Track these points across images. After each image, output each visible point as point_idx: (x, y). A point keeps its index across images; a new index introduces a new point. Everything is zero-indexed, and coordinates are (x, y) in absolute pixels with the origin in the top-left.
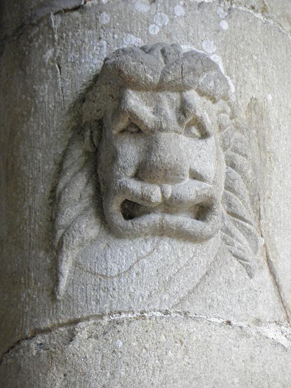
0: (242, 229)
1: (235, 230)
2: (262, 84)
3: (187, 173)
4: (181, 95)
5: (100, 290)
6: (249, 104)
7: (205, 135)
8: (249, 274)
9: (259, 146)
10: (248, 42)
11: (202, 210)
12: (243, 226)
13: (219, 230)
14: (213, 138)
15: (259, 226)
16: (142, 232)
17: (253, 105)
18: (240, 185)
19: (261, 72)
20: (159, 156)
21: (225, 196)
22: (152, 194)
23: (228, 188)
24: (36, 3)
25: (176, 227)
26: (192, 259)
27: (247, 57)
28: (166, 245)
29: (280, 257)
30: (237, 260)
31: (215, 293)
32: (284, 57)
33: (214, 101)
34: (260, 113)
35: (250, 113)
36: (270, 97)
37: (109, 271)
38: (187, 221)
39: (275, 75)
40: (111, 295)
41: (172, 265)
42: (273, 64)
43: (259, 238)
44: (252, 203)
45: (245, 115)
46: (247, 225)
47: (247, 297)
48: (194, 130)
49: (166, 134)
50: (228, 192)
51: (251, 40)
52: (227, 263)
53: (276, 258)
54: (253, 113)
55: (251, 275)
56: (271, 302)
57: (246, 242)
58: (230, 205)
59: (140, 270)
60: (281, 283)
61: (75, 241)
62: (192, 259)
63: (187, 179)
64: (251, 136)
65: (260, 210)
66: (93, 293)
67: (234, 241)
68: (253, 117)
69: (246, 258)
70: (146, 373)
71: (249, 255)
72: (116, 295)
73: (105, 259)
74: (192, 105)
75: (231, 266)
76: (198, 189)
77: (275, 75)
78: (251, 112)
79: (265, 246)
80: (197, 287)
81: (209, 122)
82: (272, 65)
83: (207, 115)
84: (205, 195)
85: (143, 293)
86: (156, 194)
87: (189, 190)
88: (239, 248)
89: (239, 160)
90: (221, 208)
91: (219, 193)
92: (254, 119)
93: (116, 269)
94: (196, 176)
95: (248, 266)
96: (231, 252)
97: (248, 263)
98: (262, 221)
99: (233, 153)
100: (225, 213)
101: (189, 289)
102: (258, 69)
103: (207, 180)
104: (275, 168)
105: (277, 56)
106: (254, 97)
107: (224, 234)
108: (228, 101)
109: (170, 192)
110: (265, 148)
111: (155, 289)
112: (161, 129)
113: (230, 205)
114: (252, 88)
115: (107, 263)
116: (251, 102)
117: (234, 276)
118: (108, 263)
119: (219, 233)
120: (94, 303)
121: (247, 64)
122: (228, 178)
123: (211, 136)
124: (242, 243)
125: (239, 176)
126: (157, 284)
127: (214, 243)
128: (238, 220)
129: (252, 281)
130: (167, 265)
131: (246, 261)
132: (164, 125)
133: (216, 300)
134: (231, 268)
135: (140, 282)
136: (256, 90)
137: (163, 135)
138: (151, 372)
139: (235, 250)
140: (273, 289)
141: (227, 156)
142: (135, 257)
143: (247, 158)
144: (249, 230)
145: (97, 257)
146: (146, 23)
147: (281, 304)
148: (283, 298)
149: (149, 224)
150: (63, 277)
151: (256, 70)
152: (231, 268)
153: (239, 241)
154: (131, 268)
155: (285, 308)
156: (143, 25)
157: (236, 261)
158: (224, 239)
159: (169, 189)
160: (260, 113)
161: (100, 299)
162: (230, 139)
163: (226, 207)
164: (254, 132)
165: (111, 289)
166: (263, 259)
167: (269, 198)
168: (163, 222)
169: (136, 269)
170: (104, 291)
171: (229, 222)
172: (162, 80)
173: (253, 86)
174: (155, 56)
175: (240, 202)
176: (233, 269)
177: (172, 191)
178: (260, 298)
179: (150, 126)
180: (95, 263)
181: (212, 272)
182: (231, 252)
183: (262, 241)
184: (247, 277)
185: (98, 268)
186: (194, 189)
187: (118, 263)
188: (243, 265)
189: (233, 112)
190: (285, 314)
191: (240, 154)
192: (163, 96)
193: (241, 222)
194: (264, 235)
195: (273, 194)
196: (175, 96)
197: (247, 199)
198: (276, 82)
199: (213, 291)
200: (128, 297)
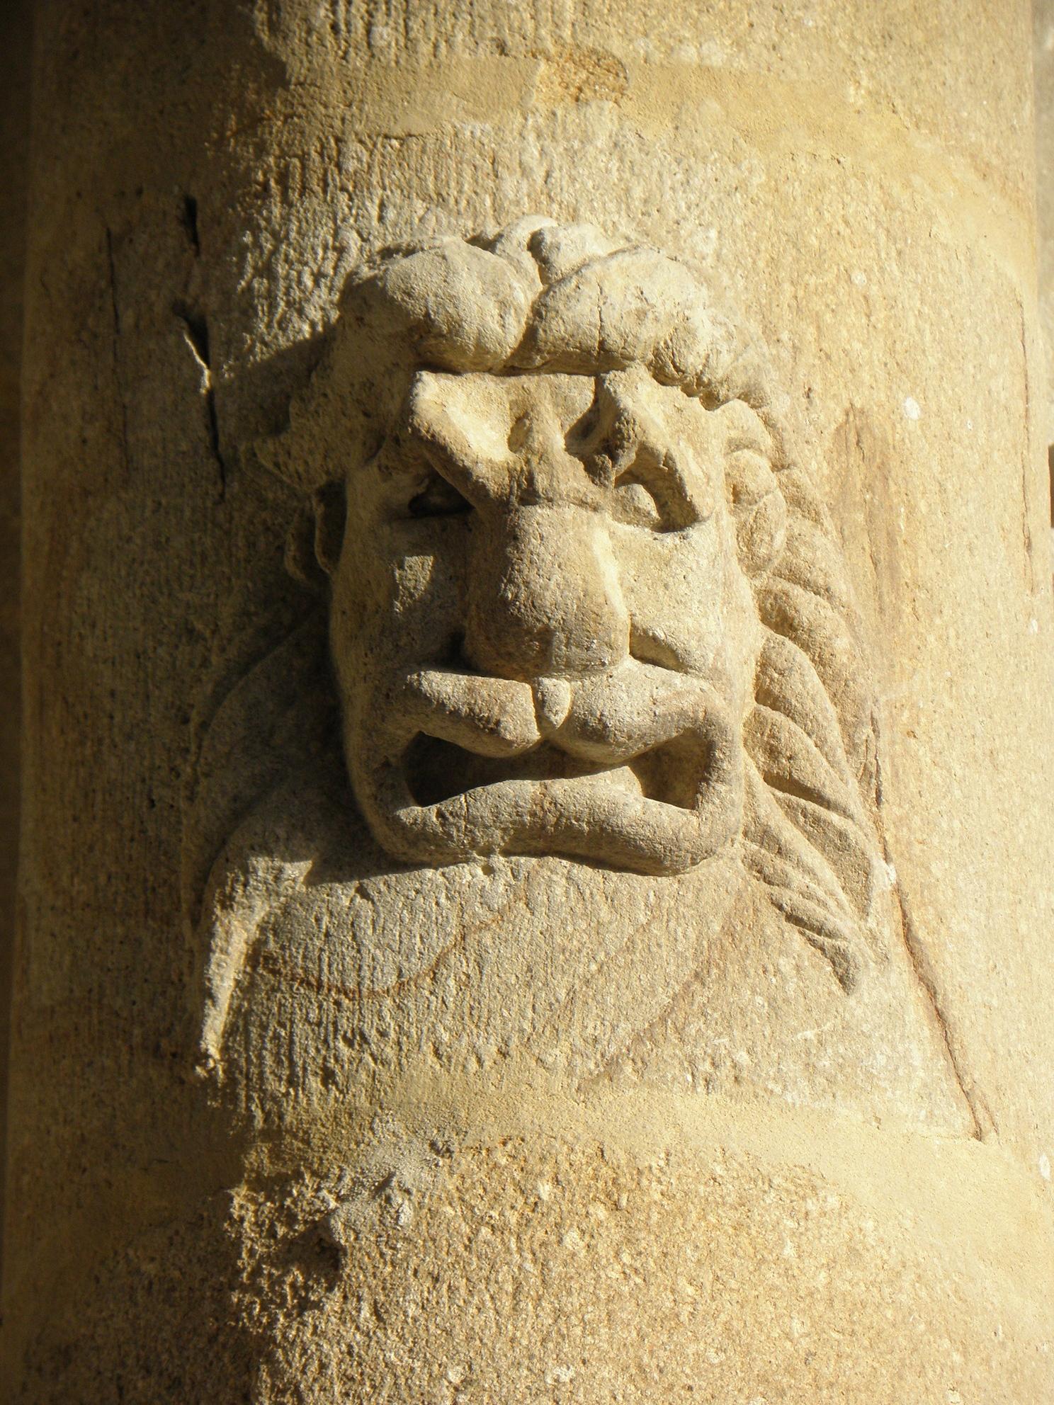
0: (816, 830)
1: (790, 834)
2: (886, 365)
3: (623, 641)
4: (599, 383)
5: (335, 1038)
6: (838, 430)
7: (676, 514)
8: (841, 980)
9: (875, 564)
10: (835, 226)
11: (678, 765)
12: (817, 821)
13: (735, 833)
14: (709, 526)
15: (877, 822)
16: (474, 844)
17: (856, 434)
18: (805, 682)
19: (879, 326)
20: (527, 584)
21: (757, 723)
22: (503, 709)
23: (765, 696)
24: (325, 477)
25: (588, 823)
26: (645, 928)
27: (830, 278)
28: (557, 874)
29: (949, 928)
30: (803, 934)
31: (725, 1040)
32: (959, 282)
33: (712, 401)
34: (878, 460)
35: (843, 458)
36: (912, 408)
37: (368, 974)
38: (617, 793)
39: (928, 337)
40: (372, 1055)
41: (580, 951)
42: (922, 301)
43: (875, 862)
44: (852, 749)
45: (825, 464)
46: (834, 817)
47: (837, 1053)
48: (645, 500)
49: (548, 511)
50: (767, 711)
51: (847, 223)
52: (764, 943)
53: (935, 932)
54: (855, 457)
55: (845, 981)
56: (921, 1074)
57: (827, 873)
58: (773, 753)
59: (472, 970)
60: (953, 1013)
61: (252, 882)
62: (645, 928)
63: (629, 664)
64: (846, 533)
65: (878, 771)
66: (312, 1052)
67: (789, 869)
68: (855, 470)
69: (829, 926)
70: (489, 1304)
71: (842, 919)
72: (390, 1052)
73: (354, 937)
74: (534, 303)
75: (781, 953)
76: (662, 693)
77: (928, 337)
78: (848, 453)
79: (898, 890)
80: (663, 1020)
81: (702, 478)
82: (918, 304)
83: (691, 452)
84: (682, 713)
85: (481, 1042)
86: (515, 708)
87: (634, 698)
88: (807, 895)
89: (805, 605)
90: (741, 766)
91: (734, 710)
92: (858, 480)
93: (390, 968)
94: (651, 650)
95: (838, 951)
96: (780, 908)
97: (838, 943)
98: (890, 811)
99: (787, 586)
100: (758, 779)
101: (638, 1025)
102: (868, 316)
103: (692, 663)
104: (931, 638)
105: (935, 278)
106: (858, 405)
107: (755, 847)
108: (764, 409)
109: (567, 704)
110: (893, 569)
111: (522, 1031)
112: (530, 496)
113: (773, 753)
114: (850, 375)
115: (359, 951)
116: (847, 421)
117: (791, 987)
118: (363, 950)
119: (737, 845)
120: (315, 1083)
121: (831, 298)
122: (765, 664)
123: (704, 520)
124: (815, 876)
125: (803, 658)
126: (530, 1014)
127: (724, 874)
128: (802, 802)
129: (852, 1002)
130: (563, 951)
131: (830, 935)
132: (541, 482)
133: (729, 1063)
134: (782, 961)
135: (472, 1008)
136: (862, 383)
137: (539, 514)
138: (507, 1303)
139: (789, 898)
140: (927, 1032)
141: (763, 594)
142: (453, 929)
143: (830, 598)
144: (842, 835)
145: (327, 935)
146: (488, 165)
147: (955, 1079)
148: (959, 1060)
149: (496, 815)
150: (214, 1004)
151: (864, 320)
152: (782, 961)
153: (809, 871)
154: (441, 960)
155: (967, 1094)
156: (479, 173)
157: (797, 936)
158: (756, 867)
159: (563, 692)
160: (878, 460)
161: (337, 1069)
162: (772, 537)
163: (762, 758)
164: (860, 517)
165: (373, 1035)
166: (889, 933)
167: (912, 734)
168: (547, 805)
169: (460, 965)
170: (350, 1043)
171: (769, 802)
172: (531, 335)
173: (852, 371)
174: (509, 257)
175: (810, 742)
176: (786, 965)
177: (573, 703)
178: (882, 1060)
179: (492, 487)
180: (321, 950)
181: (715, 971)
182: (780, 908)
183: (884, 876)
184: (836, 987)
185: (330, 966)
186: (648, 694)
187: (396, 946)
188: (822, 949)
189: (780, 449)
190: (967, 1114)
191: (806, 585)
192: (539, 386)
193: (811, 806)
194: (894, 856)
195: (923, 720)
196: (581, 392)
197: (835, 734)
198: (932, 361)
199: (719, 1035)
200: (431, 1059)
